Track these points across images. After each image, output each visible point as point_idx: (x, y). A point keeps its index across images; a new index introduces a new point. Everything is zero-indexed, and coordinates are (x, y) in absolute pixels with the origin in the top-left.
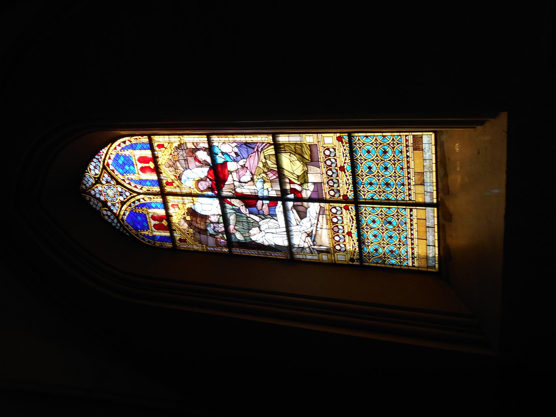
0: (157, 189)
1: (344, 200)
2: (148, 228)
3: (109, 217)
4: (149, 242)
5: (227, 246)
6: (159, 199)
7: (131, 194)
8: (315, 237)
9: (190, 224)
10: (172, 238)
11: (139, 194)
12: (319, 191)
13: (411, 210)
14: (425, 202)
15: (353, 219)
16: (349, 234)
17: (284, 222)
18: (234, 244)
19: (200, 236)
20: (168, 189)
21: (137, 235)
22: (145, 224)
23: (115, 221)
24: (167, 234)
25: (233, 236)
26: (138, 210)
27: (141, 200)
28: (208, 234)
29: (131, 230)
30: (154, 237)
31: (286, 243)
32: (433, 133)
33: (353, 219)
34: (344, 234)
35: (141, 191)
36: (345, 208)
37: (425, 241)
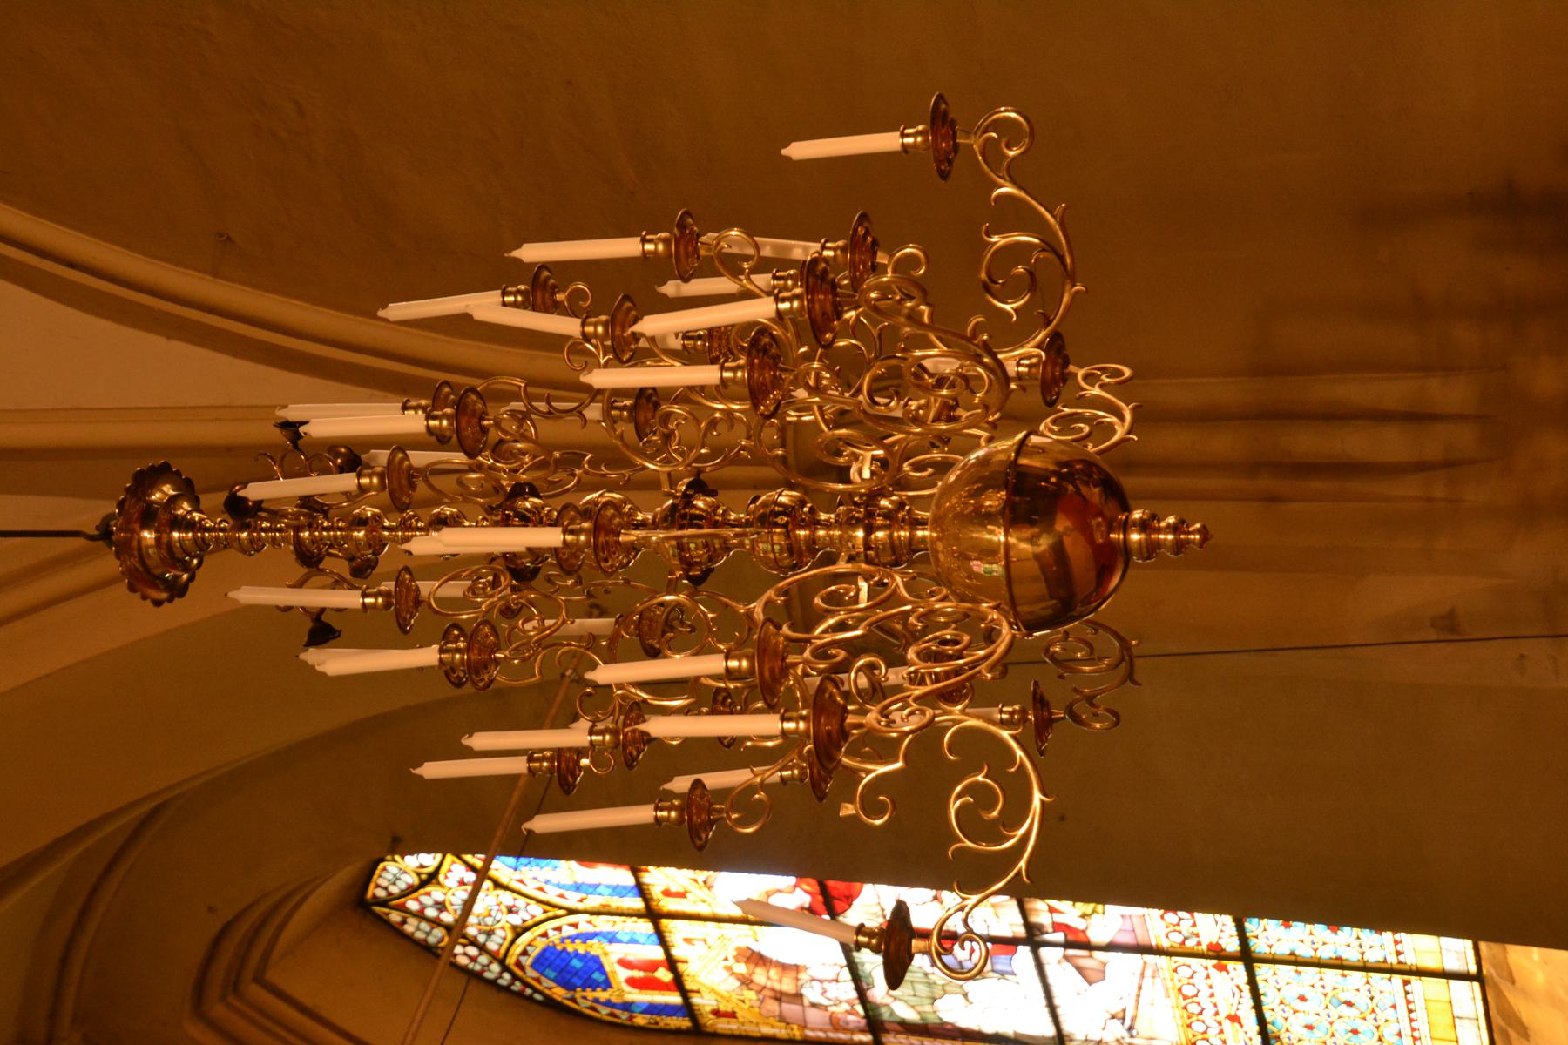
0: (638, 904)
1: (1211, 953)
2: (607, 985)
3: (474, 959)
4: (611, 1014)
5: (867, 1029)
6: (646, 927)
7: (545, 912)
8: (1133, 1020)
9: (746, 982)
10: (688, 1009)
11: (571, 912)
12: (1136, 930)
13: (1406, 983)
14: (1444, 969)
15: (1241, 991)
16: (1234, 1019)
17: (57, 529)
18: (887, 1026)
19: (780, 1006)
20: (669, 905)
21: (573, 1000)
22: (597, 976)
23: (495, 968)
24: (675, 999)
25: (883, 1010)
26: (575, 946)
27: (551, 933)
28: (806, 1003)
29: (550, 989)
30: (627, 1006)
31: (1050, 1031)
32: (456, 921)
33: (1241, 991)
34: (1218, 1018)
35: (580, 906)
36: (1217, 967)
37: (1434, 1036)
